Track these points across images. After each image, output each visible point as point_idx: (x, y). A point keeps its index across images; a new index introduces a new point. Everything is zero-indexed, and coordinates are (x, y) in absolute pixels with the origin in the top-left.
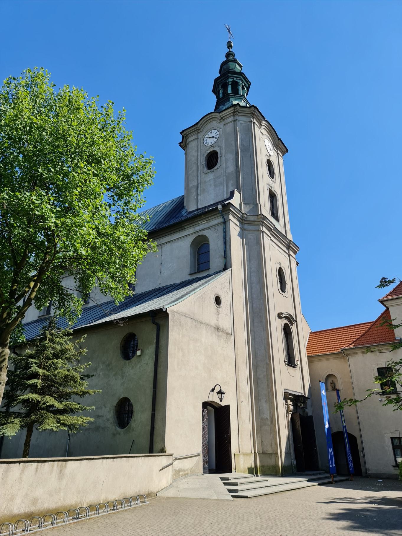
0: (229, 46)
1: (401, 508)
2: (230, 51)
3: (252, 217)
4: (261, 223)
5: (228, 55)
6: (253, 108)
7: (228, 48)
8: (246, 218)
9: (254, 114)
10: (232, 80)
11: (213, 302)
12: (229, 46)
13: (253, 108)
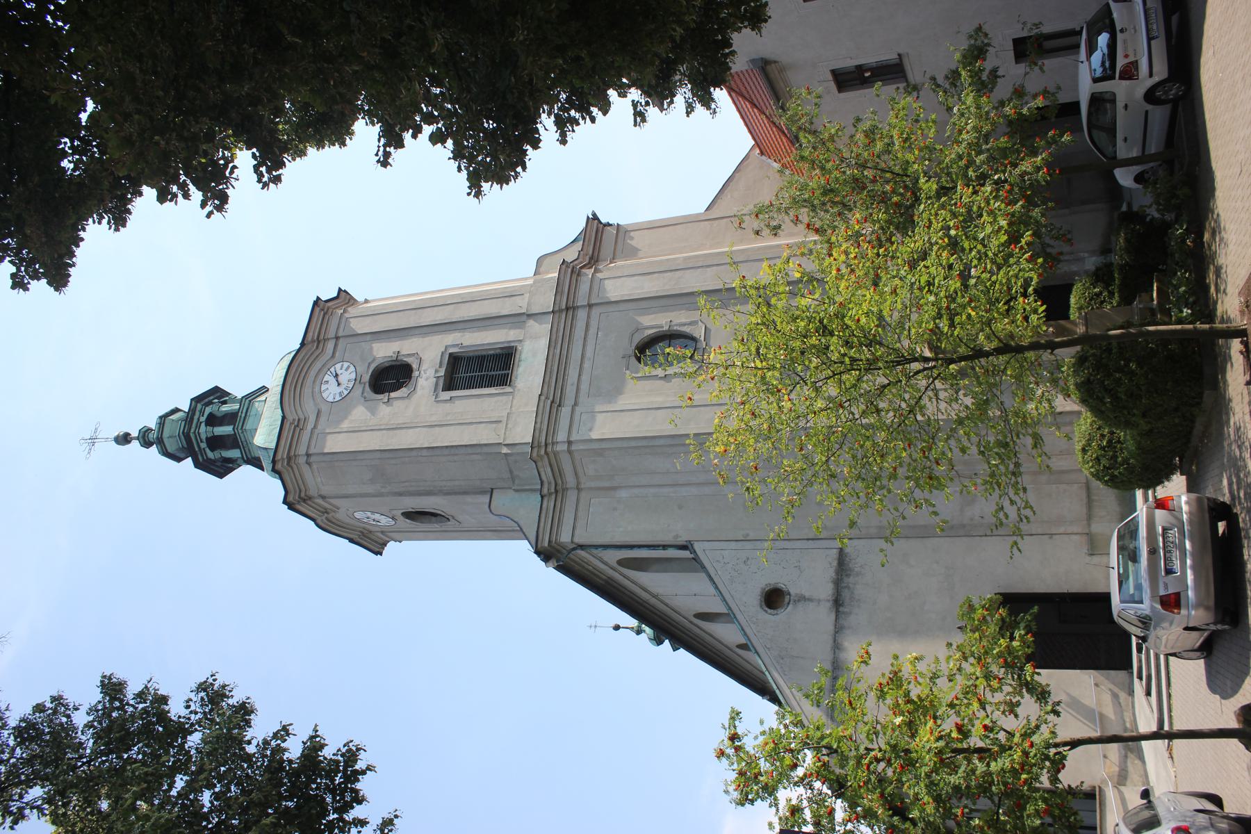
0: (124, 439)
1: (1139, 494)
2: (138, 438)
3: (543, 474)
4: (549, 449)
5: (147, 444)
6: (279, 466)
7: (129, 442)
8: (549, 483)
9: (289, 458)
10: (208, 450)
11: (783, 615)
12: (124, 439)
13: (279, 466)
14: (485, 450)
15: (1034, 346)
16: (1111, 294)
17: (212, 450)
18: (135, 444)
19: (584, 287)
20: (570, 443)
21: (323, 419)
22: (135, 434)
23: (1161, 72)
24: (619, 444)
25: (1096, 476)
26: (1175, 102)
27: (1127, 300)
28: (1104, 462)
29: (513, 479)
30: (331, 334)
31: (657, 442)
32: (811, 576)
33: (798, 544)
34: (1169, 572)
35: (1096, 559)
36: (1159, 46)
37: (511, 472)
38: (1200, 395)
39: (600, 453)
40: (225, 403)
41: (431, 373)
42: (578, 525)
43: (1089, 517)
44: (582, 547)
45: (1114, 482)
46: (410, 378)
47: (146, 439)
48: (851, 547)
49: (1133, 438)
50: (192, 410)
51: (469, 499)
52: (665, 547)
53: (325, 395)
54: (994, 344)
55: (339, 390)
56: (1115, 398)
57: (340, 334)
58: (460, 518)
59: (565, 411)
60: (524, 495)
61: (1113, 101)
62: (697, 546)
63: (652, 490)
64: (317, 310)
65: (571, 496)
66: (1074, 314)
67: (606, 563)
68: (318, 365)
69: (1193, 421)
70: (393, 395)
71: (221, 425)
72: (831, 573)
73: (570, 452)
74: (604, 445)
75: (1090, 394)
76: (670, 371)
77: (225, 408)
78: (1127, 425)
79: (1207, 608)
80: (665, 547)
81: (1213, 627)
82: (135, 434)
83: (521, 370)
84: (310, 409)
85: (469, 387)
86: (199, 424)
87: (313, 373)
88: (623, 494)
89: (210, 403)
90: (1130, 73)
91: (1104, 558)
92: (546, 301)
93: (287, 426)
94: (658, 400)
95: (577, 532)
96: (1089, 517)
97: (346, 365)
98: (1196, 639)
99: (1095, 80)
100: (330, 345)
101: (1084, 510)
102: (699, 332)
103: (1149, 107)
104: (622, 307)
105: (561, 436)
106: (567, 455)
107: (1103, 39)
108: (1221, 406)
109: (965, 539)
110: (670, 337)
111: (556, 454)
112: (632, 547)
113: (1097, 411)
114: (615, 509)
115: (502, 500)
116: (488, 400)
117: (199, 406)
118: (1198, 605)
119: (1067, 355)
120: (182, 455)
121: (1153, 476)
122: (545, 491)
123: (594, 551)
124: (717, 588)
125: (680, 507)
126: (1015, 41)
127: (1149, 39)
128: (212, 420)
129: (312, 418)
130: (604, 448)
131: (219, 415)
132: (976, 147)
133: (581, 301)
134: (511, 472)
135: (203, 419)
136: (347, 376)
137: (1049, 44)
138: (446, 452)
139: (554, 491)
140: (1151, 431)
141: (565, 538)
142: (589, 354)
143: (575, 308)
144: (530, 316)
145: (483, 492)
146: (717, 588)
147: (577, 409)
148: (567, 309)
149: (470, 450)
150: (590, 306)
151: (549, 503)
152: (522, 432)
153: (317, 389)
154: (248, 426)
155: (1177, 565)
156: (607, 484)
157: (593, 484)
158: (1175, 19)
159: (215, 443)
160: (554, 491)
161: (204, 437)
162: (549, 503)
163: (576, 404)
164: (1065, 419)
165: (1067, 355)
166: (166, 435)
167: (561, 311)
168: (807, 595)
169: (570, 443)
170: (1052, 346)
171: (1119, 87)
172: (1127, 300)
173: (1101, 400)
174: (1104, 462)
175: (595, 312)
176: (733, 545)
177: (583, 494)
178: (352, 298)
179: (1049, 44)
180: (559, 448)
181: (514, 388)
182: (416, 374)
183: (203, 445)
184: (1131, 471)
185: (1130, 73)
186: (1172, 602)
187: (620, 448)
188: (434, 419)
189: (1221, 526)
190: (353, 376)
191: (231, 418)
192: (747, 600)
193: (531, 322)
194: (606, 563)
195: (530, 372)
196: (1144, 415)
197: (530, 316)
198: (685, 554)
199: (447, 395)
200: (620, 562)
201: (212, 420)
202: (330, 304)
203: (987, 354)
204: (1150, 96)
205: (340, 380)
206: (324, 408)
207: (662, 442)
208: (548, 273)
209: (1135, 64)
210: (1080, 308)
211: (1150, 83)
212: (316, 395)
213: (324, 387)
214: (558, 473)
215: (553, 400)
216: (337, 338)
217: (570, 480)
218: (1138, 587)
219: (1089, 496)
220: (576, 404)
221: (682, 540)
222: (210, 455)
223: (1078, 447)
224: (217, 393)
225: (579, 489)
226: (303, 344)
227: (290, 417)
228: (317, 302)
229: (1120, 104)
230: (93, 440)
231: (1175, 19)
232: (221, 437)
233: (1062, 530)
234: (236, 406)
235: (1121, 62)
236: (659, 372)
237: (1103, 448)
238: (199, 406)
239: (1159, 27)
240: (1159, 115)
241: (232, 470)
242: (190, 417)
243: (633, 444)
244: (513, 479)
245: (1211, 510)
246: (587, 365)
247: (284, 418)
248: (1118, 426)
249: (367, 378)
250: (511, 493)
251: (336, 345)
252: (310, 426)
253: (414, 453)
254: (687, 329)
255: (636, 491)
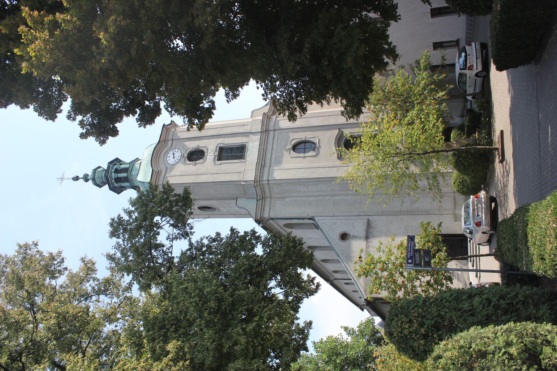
0: (76, 178)
2: (83, 178)
12: (76, 178)
14: (236, 183)
15: (442, 151)
16: (464, 134)
17: (116, 183)
18: (81, 181)
19: (272, 123)
20: (268, 180)
21: (168, 171)
22: (81, 176)
23: (480, 68)
24: (287, 181)
25: (458, 191)
26: (484, 77)
27: (469, 136)
28: (460, 186)
29: (245, 194)
30: (170, 138)
31: (302, 181)
32: (359, 228)
33: (353, 217)
34: (478, 216)
35: (457, 223)
36: (479, 61)
37: (245, 191)
38: (489, 166)
39: (279, 184)
40: (121, 164)
41: (212, 154)
42: (271, 211)
43: (455, 208)
44: (272, 219)
45: (463, 193)
46: (204, 155)
47: (86, 178)
48: (370, 218)
49: (469, 178)
50: (109, 167)
51: (227, 201)
52: (303, 219)
53: (169, 162)
54: (431, 150)
55: (174, 160)
56: (464, 166)
57: (174, 138)
58: (221, 209)
59: (266, 169)
60: (249, 200)
61: (466, 75)
62: (316, 218)
63: (298, 198)
64: (164, 129)
65: (268, 200)
66: (452, 140)
67: (279, 226)
68: (165, 150)
69: (487, 174)
70: (197, 162)
71: (121, 173)
72: (365, 228)
73: (268, 184)
74: (281, 182)
75: (458, 165)
76: (306, 155)
77: (122, 166)
78: (467, 174)
79: (488, 226)
80: (303, 219)
81: (490, 232)
82: (81, 176)
83: (248, 153)
84: (162, 167)
85: (514, 165)
86: (111, 172)
87: (163, 153)
88: (288, 199)
89: (115, 164)
90: (471, 68)
91: (460, 223)
92: (258, 128)
93: (154, 173)
94: (302, 165)
95: (271, 213)
96: (455, 208)
97: (177, 150)
98: (486, 237)
99: (461, 69)
100: (170, 143)
101: (453, 206)
102: (316, 141)
103: (477, 78)
104: (287, 131)
105: (265, 178)
106: (267, 185)
107: (463, 54)
108: (494, 169)
109: (412, 216)
110: (305, 142)
111: (263, 185)
112: (291, 219)
113: (459, 170)
114: (285, 205)
115: (241, 202)
116: (237, 164)
117: (111, 165)
118: (485, 225)
119: (451, 153)
120: (101, 185)
121: (475, 191)
122: (258, 198)
123: (276, 221)
124: (323, 233)
125: (309, 204)
126: (434, 43)
127: (477, 58)
128: (117, 171)
129: (164, 171)
130: (281, 183)
131: (119, 169)
132: (424, 89)
133: (271, 128)
134: (245, 191)
135: (113, 171)
136: (178, 154)
137: (445, 45)
138: (220, 184)
139: (261, 198)
140: (474, 177)
141: (266, 215)
142: (275, 148)
143: (268, 131)
144: (251, 133)
145: (233, 199)
146: (323, 233)
147: (271, 168)
148: (266, 131)
149: (229, 183)
150: (275, 130)
151: (260, 203)
152: (250, 176)
153: (165, 159)
154: (134, 173)
155: (480, 214)
156: (281, 196)
157: (276, 196)
158: (484, 51)
159: (118, 180)
160: (261, 198)
161: (113, 178)
162: (260, 203)
163: (270, 166)
164: (449, 173)
165: (451, 153)
166: (96, 176)
167: (263, 132)
168: (356, 235)
169: (268, 180)
170: (447, 151)
171: (467, 72)
172: (469, 136)
173: (460, 167)
174: (460, 186)
175: (277, 132)
176: (329, 218)
177: (272, 200)
178: (176, 124)
179: (445, 45)
180: (264, 182)
181: (246, 160)
182: (206, 154)
183: (113, 181)
184: (469, 190)
185: (471, 68)
186: (478, 224)
187: (287, 183)
188: (214, 171)
189: (493, 204)
190: (180, 155)
191: (126, 170)
192: (335, 237)
193: (251, 136)
194: (279, 226)
195: (252, 154)
196: (472, 172)
197: (251, 133)
198: (311, 221)
199: (219, 162)
200: (285, 225)
201: (117, 171)
202: (169, 126)
203: (429, 153)
204: (477, 75)
205: (174, 156)
206: (168, 167)
207: (303, 181)
208: (256, 117)
209: (472, 66)
210: (454, 138)
211: (477, 71)
212: (165, 162)
213: (168, 159)
214: (263, 192)
215: (261, 165)
216: (173, 140)
217: (268, 194)
218: (470, 242)
219: (455, 201)
220: (270, 166)
221: (310, 216)
222: (116, 185)
223: (453, 182)
224: (117, 161)
225: (271, 198)
226: (159, 142)
227: (155, 170)
228: (164, 125)
229: (468, 77)
230: (62, 179)
231: (484, 51)
232: (120, 178)
233: (445, 213)
234: (128, 166)
235: (468, 65)
236: (302, 155)
237: (460, 182)
238: (111, 165)
239: (479, 55)
240: (479, 80)
241: (122, 191)
242: (107, 171)
243: (292, 181)
244: (245, 194)
245: (490, 198)
246: (274, 152)
247: (153, 170)
248: (465, 174)
249: (186, 155)
250: (244, 199)
251: (172, 143)
252: (163, 174)
253: (207, 184)
254: (312, 140)
255: (293, 198)
